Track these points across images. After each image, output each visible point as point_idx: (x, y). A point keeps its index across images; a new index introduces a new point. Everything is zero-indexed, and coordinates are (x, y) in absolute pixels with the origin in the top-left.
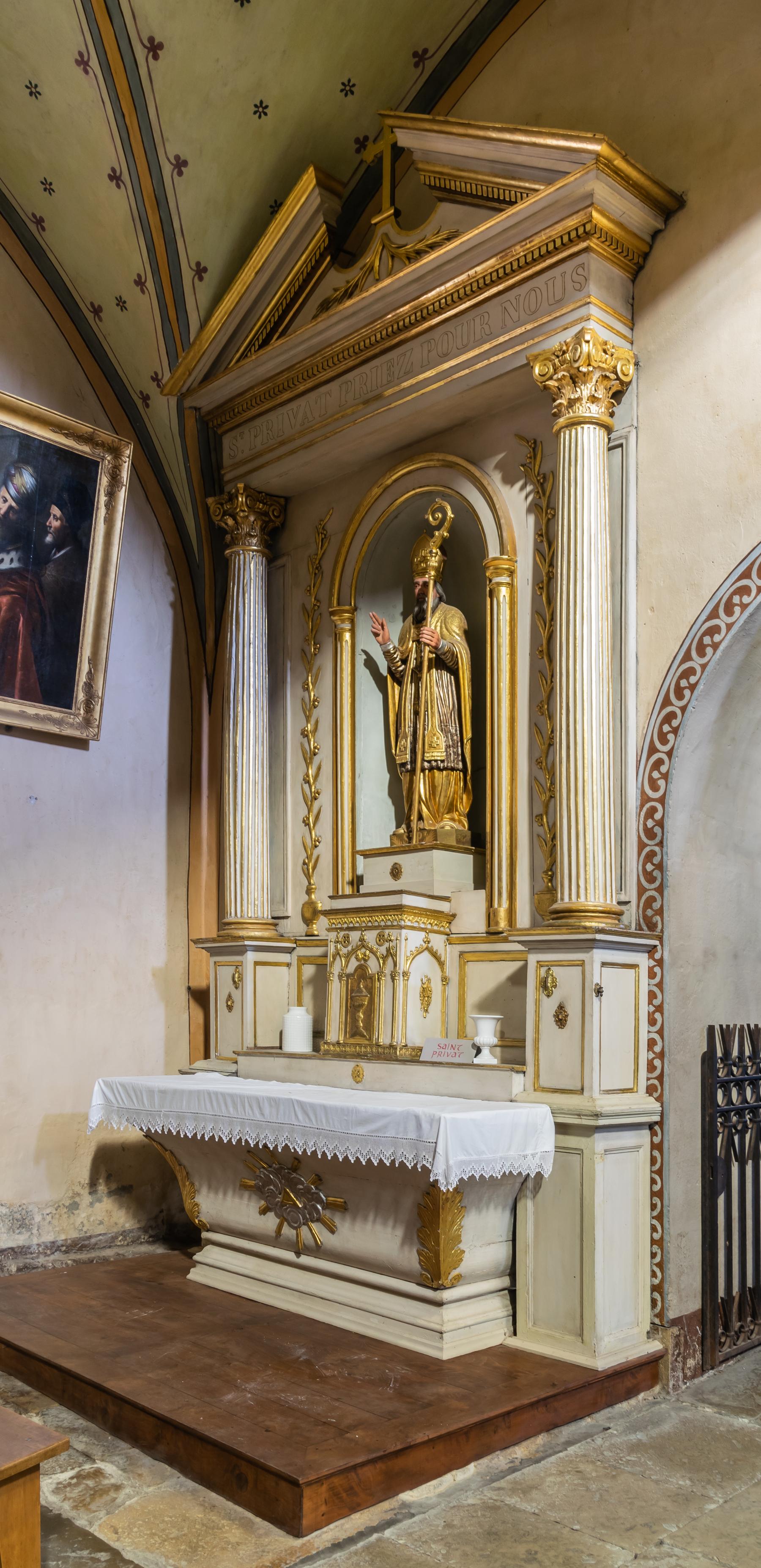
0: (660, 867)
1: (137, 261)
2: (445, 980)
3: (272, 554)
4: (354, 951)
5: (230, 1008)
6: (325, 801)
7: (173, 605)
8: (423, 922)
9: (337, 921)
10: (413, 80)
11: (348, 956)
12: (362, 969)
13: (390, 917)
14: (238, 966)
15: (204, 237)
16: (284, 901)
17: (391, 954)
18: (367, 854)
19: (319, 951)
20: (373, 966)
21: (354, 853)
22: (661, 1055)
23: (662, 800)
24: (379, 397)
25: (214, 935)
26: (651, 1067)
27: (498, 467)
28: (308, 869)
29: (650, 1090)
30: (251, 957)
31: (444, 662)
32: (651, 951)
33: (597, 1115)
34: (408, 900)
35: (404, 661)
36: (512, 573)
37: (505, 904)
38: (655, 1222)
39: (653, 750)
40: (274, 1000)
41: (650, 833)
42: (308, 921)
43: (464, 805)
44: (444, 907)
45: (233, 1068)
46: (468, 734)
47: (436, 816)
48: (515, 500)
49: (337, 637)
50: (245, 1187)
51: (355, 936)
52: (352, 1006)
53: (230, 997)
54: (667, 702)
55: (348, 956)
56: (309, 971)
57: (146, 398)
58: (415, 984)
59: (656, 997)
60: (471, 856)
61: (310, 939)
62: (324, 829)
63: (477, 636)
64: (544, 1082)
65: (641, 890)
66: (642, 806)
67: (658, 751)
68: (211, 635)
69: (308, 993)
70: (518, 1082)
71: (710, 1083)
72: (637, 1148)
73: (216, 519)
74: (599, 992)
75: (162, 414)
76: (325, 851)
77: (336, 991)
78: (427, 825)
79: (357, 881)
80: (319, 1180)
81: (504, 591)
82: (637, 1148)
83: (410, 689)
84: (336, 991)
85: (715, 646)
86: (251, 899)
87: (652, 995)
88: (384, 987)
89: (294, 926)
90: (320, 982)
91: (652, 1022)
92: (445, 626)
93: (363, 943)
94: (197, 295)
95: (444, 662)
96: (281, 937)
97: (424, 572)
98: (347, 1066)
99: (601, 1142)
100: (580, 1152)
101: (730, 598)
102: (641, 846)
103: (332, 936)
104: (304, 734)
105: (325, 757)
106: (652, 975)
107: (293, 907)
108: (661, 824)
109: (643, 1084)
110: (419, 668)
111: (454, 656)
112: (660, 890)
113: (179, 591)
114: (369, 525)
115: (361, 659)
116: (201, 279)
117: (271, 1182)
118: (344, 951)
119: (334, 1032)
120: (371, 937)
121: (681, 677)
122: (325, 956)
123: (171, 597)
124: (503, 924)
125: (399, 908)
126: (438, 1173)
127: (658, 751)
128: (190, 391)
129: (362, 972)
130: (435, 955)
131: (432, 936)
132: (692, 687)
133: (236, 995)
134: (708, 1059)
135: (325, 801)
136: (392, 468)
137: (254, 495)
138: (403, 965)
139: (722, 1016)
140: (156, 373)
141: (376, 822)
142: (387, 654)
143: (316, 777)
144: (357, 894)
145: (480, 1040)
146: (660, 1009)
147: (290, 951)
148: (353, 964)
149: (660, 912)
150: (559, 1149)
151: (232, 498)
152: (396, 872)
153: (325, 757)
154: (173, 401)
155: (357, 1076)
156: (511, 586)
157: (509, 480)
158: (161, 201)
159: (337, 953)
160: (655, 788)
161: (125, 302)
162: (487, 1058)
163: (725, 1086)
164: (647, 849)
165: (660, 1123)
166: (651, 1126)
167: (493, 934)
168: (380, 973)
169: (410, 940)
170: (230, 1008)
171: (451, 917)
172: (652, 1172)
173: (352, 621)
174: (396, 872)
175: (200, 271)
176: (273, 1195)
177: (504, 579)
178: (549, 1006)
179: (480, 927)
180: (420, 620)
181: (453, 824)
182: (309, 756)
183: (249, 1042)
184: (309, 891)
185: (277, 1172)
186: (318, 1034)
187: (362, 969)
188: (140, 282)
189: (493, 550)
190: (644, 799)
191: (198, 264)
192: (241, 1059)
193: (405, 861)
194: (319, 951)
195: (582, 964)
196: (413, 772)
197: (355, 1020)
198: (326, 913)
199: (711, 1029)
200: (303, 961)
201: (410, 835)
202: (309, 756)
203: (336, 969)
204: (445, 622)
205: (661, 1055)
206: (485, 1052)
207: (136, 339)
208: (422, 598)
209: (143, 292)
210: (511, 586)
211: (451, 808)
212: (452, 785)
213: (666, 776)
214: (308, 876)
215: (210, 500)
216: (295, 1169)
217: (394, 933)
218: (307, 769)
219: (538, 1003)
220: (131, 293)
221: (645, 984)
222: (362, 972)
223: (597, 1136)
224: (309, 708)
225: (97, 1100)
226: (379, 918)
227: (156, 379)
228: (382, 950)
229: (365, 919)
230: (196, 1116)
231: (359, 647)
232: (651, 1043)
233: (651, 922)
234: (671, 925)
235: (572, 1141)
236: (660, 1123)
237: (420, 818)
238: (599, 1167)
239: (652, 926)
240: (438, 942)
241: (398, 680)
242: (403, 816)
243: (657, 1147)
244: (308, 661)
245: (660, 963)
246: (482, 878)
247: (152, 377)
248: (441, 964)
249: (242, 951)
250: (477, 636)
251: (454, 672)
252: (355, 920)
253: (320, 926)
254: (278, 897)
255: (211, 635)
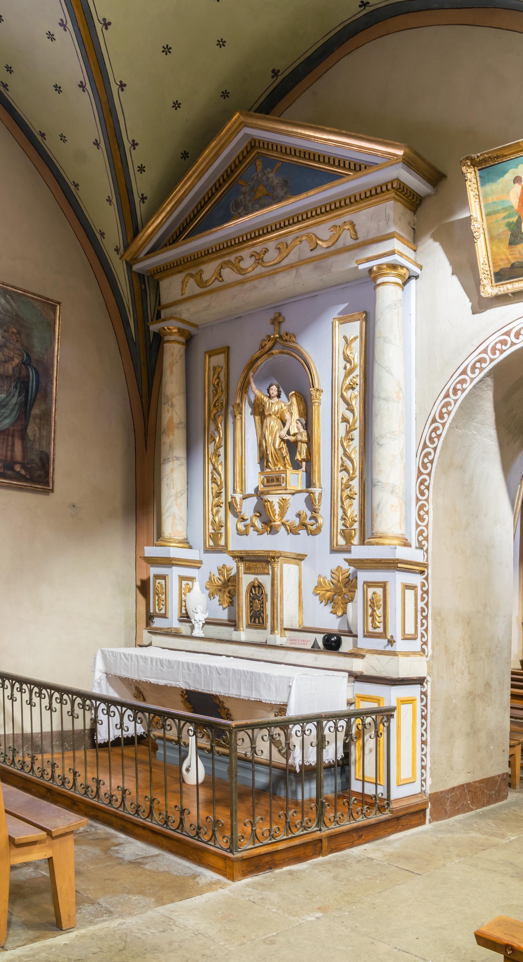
10: (265, 85)
25: (198, 551)
38: (423, 708)
59: (425, 612)
66: (418, 478)
67: (428, 447)
101: (474, 364)
116: (143, 202)
121: (443, 407)
127: (428, 447)
140: (96, 140)
146: (427, 592)
160: (426, 468)
161: (53, 35)
164: (420, 503)
172: (422, 780)
175: (143, 199)
188: (62, 24)
191: (142, 195)
209: (111, 204)
220: (58, 31)
247: (94, 143)
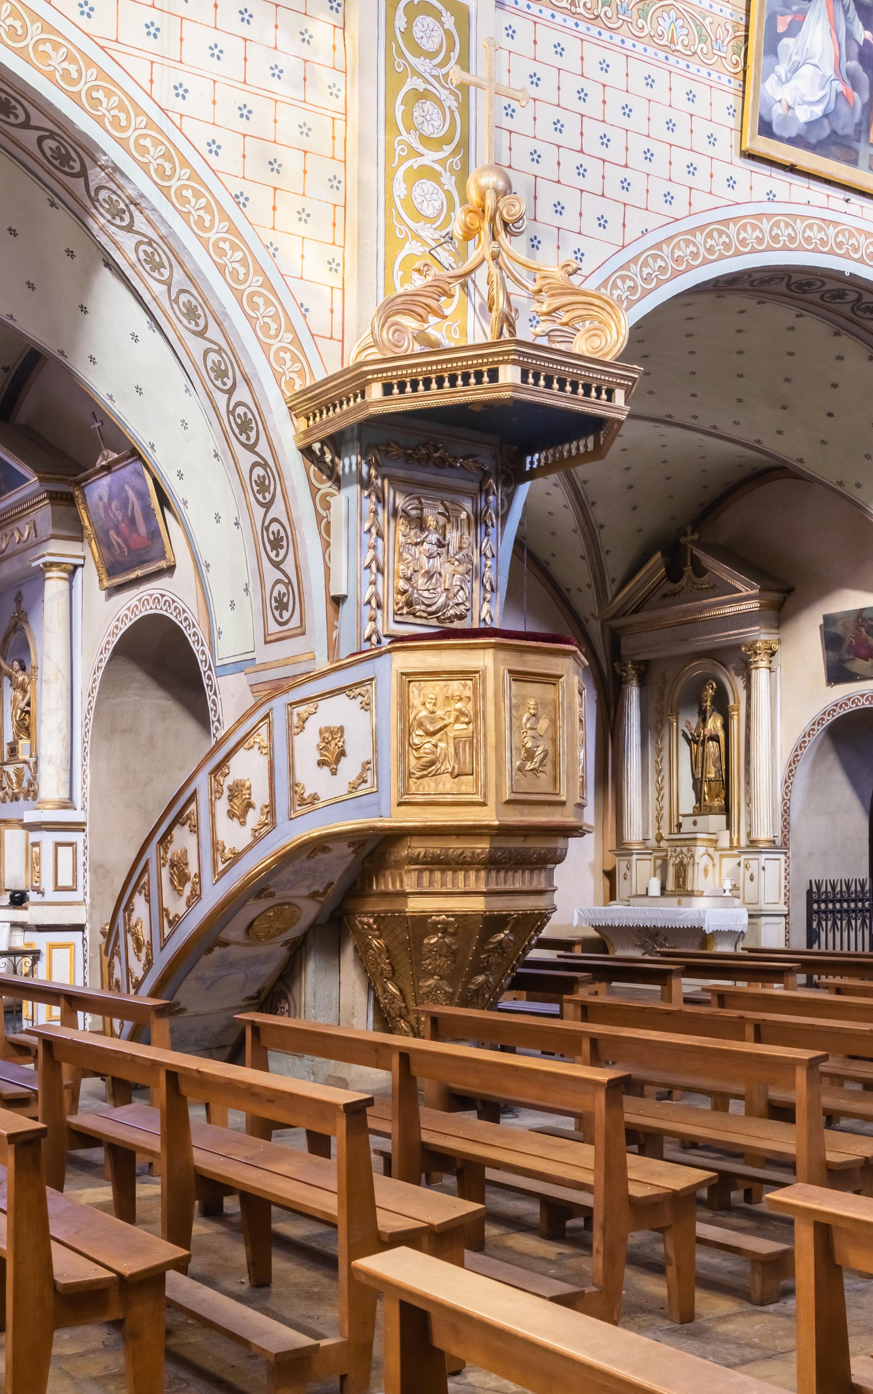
0: (788, 823)
1: (588, 579)
2: (714, 865)
3: (642, 685)
4: (678, 855)
5: (625, 879)
6: (666, 791)
7: (596, 702)
8: (705, 843)
9: (671, 843)
11: (676, 857)
12: (681, 862)
13: (692, 842)
14: (629, 861)
15: (615, 566)
16: (648, 832)
17: (692, 856)
18: (684, 816)
19: (663, 854)
20: (685, 861)
21: (678, 815)
22: (789, 891)
23: (789, 800)
24: (686, 640)
26: (785, 895)
27: (733, 668)
28: (659, 819)
29: (785, 903)
30: (635, 857)
31: (714, 738)
32: (785, 853)
33: (761, 910)
34: (699, 836)
35: (699, 736)
36: (738, 710)
37: (736, 836)
39: (786, 782)
40: (643, 875)
41: (785, 812)
42: (658, 841)
43: (723, 795)
44: (713, 837)
45: (628, 903)
46: (724, 768)
47: (711, 799)
48: (740, 683)
49: (671, 725)
50: (637, 946)
51: (678, 849)
52: (678, 876)
53: (625, 874)
54: (790, 765)
55: (676, 857)
56: (659, 862)
57: (587, 620)
58: (702, 866)
60: (167, 1294)
61: (659, 849)
62: (665, 803)
63: (726, 727)
64: (747, 901)
65: (783, 832)
68: (612, 712)
69: (658, 872)
70: (737, 901)
71: (810, 901)
72: (780, 923)
73: (618, 672)
74: (764, 869)
75: (595, 627)
76: (666, 812)
77: (671, 871)
78: (707, 803)
79: (679, 825)
80: (665, 939)
81: (735, 717)
82: (780, 923)
83: (701, 748)
84: (671, 871)
85: (805, 747)
86: (634, 832)
87: (786, 869)
88: (690, 869)
89: (652, 843)
90: (664, 867)
91: (786, 879)
92: (714, 724)
93: (682, 852)
94: (611, 589)
95: (714, 738)
96: (647, 848)
97: (707, 701)
98: (676, 899)
99: (764, 920)
100: (756, 924)
102: (783, 816)
103: (669, 849)
104: (657, 762)
105: (665, 772)
106: (786, 862)
107: (652, 835)
108: (789, 808)
109: (783, 901)
110: (704, 740)
111: (718, 736)
112: (788, 832)
113: (599, 695)
114: (683, 680)
115: (680, 733)
117: (647, 942)
118: (674, 855)
119: (670, 886)
120: (685, 849)
122: (667, 856)
123: (595, 698)
124: (735, 844)
125: (695, 839)
126: (705, 928)
128: (607, 620)
129: (681, 863)
130: (710, 856)
131: (709, 849)
132: (798, 761)
133: (628, 873)
134: (809, 893)
135: (666, 791)
136: (691, 661)
137: (635, 663)
138: (697, 860)
139: (816, 876)
141: (687, 801)
142: (691, 734)
143: (662, 781)
144: (679, 832)
145: (725, 887)
146: (788, 874)
147: (650, 854)
148: (678, 860)
149: (788, 840)
150: (749, 924)
151: (625, 665)
152: (695, 823)
153: (665, 772)
154: (599, 623)
155: (679, 903)
156: (738, 715)
157: (737, 675)
158: (600, 564)
159: (672, 856)
162: (728, 893)
163: (817, 902)
165: (788, 915)
166: (785, 916)
167: (732, 848)
168: (688, 863)
169: (700, 850)
170: (625, 879)
171: (716, 841)
173: (677, 718)
174: (695, 823)
176: (648, 947)
177: (735, 713)
178: (748, 874)
179: (727, 845)
180: (704, 721)
181: (718, 803)
182: (659, 772)
183: (634, 893)
184: (659, 829)
185: (649, 938)
186: (663, 888)
187: (681, 862)
189: (731, 703)
190: (784, 799)
192: (631, 900)
193: (699, 819)
194: (663, 854)
195: (758, 859)
196: (701, 782)
197: (679, 882)
198: (667, 840)
199: (811, 881)
200: (656, 858)
201: (701, 809)
202: (659, 772)
203: (671, 862)
204: (714, 722)
205: (789, 891)
206: (727, 891)
207: (586, 603)
208: (705, 712)
210: (738, 715)
211: (717, 796)
212: (717, 786)
213: (790, 791)
214: (659, 822)
215: (615, 664)
216: (657, 935)
217: (693, 848)
218: (658, 773)
219: (744, 873)
221: (783, 866)
222: (681, 863)
223: (762, 918)
224: (659, 751)
225: (576, 916)
226: (688, 843)
227: (592, 615)
228: (689, 855)
229: (683, 843)
230: (619, 919)
231: (680, 728)
232: (786, 886)
233: (785, 844)
234: (792, 844)
235: (754, 920)
236: (788, 915)
237: (705, 800)
238: (763, 929)
239: (786, 845)
240: (711, 851)
241: (696, 742)
242: (699, 799)
243: (787, 923)
244: (658, 732)
245: (788, 858)
246: (729, 826)
248: (712, 859)
249: (631, 855)
250: (726, 727)
251: (718, 741)
252: (679, 843)
253: (663, 844)
254: (646, 831)
255: (612, 712)
